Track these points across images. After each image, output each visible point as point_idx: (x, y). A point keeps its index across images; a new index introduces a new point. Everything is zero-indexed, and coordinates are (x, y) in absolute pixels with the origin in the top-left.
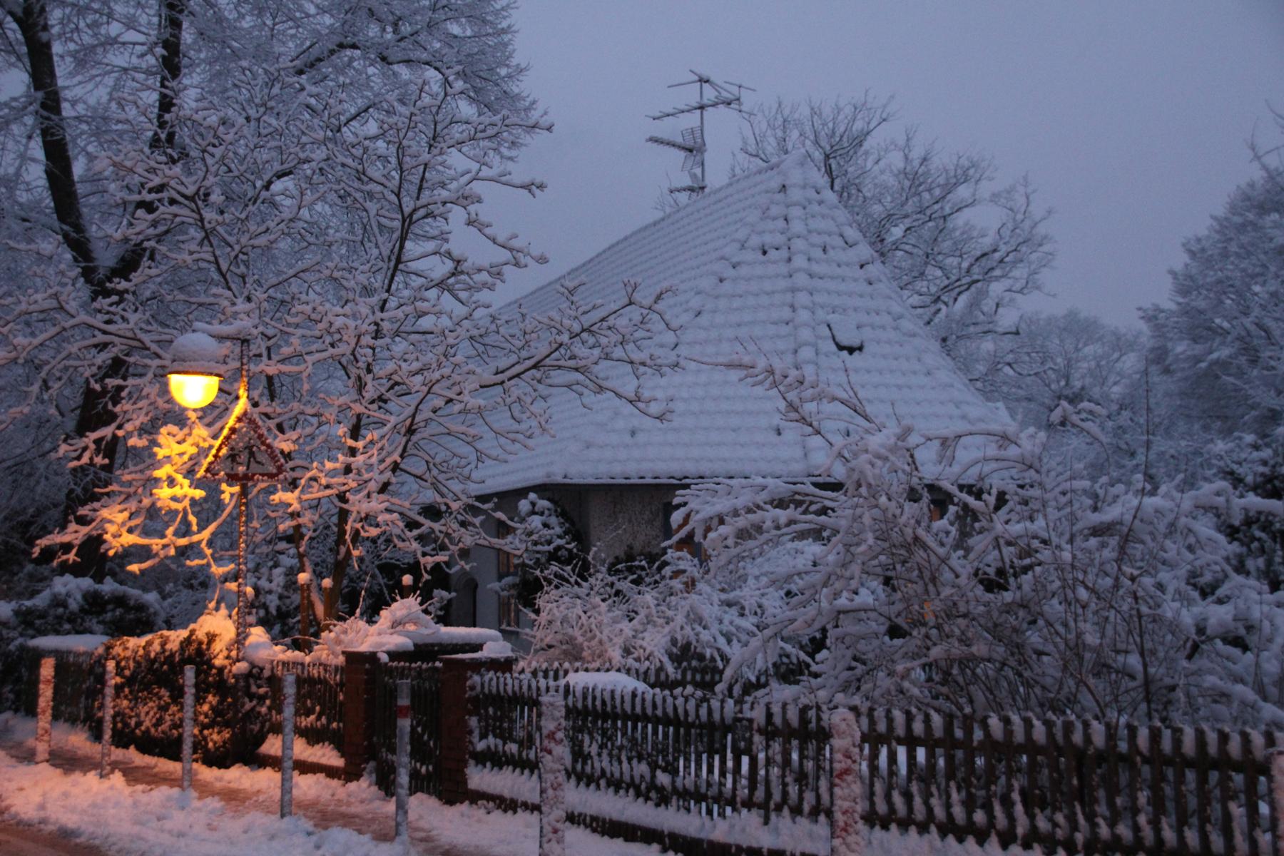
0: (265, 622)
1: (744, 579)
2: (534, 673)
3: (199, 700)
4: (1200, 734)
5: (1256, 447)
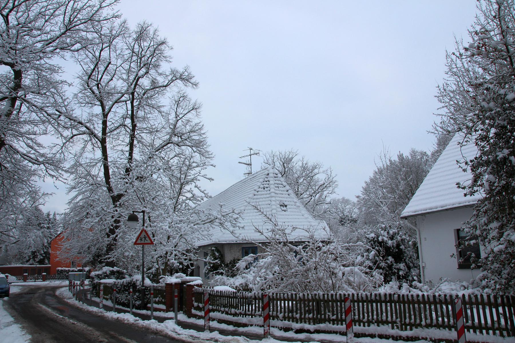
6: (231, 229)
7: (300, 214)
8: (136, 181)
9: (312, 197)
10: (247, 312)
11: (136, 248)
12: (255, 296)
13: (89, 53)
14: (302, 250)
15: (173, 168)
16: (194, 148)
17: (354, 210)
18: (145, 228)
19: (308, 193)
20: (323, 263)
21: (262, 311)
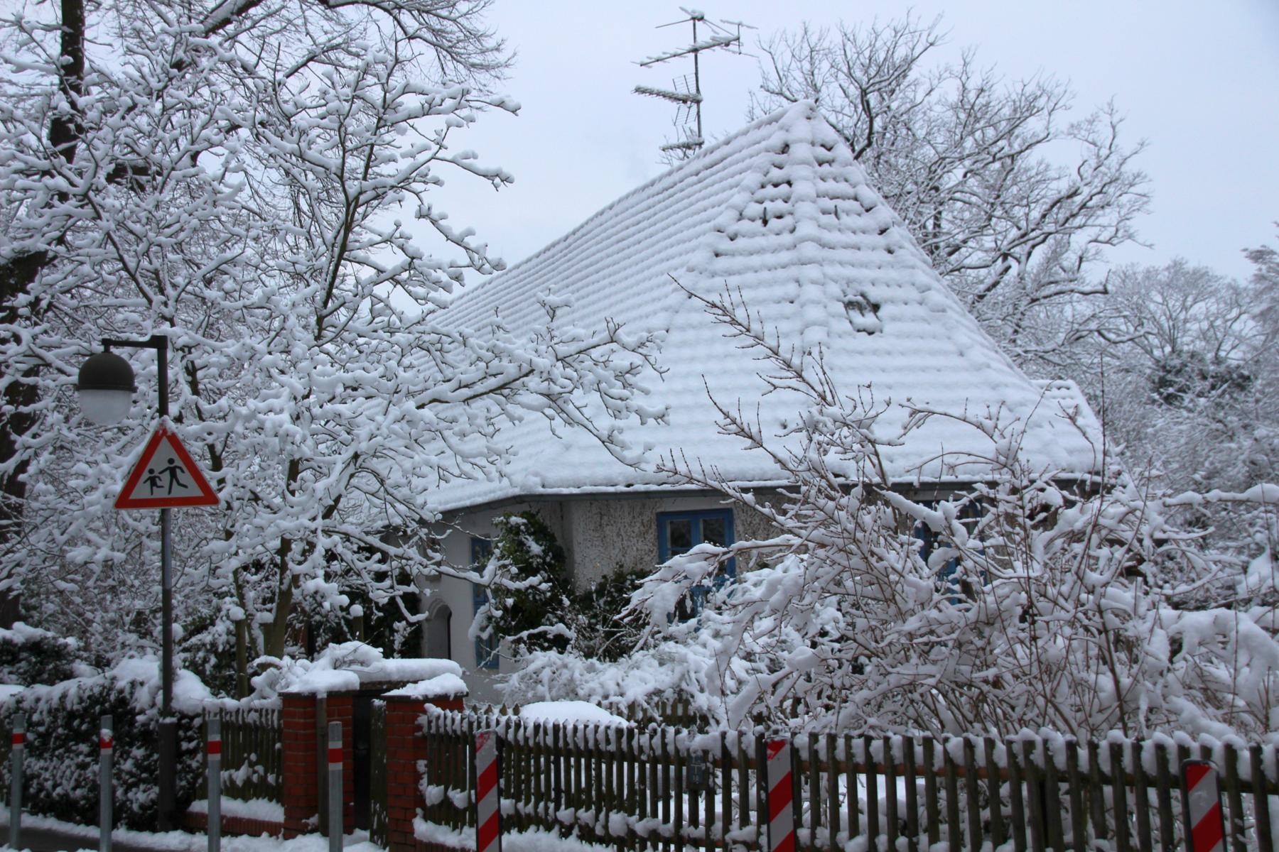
6: (604, 423)
7: (950, 347)
8: (112, 188)
9: (1011, 261)
10: (687, 830)
11: (125, 527)
12: (724, 748)
14: (956, 524)
15: (301, 120)
16: (405, 17)
17: (1236, 326)
18: (171, 426)
19: (988, 242)
20: (1065, 589)
21: (760, 822)
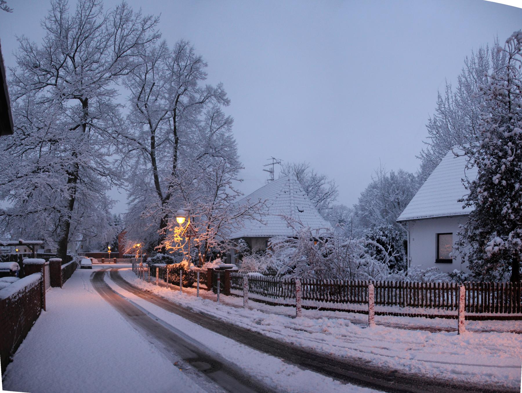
0: (193, 262)
1: (281, 255)
2: (242, 272)
3: (182, 276)
4: (359, 281)
5: (371, 231)
13: (137, 77)
